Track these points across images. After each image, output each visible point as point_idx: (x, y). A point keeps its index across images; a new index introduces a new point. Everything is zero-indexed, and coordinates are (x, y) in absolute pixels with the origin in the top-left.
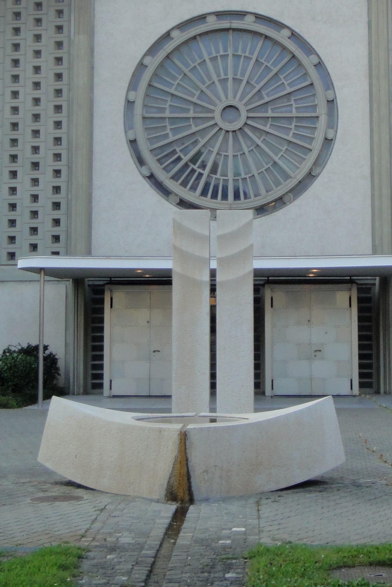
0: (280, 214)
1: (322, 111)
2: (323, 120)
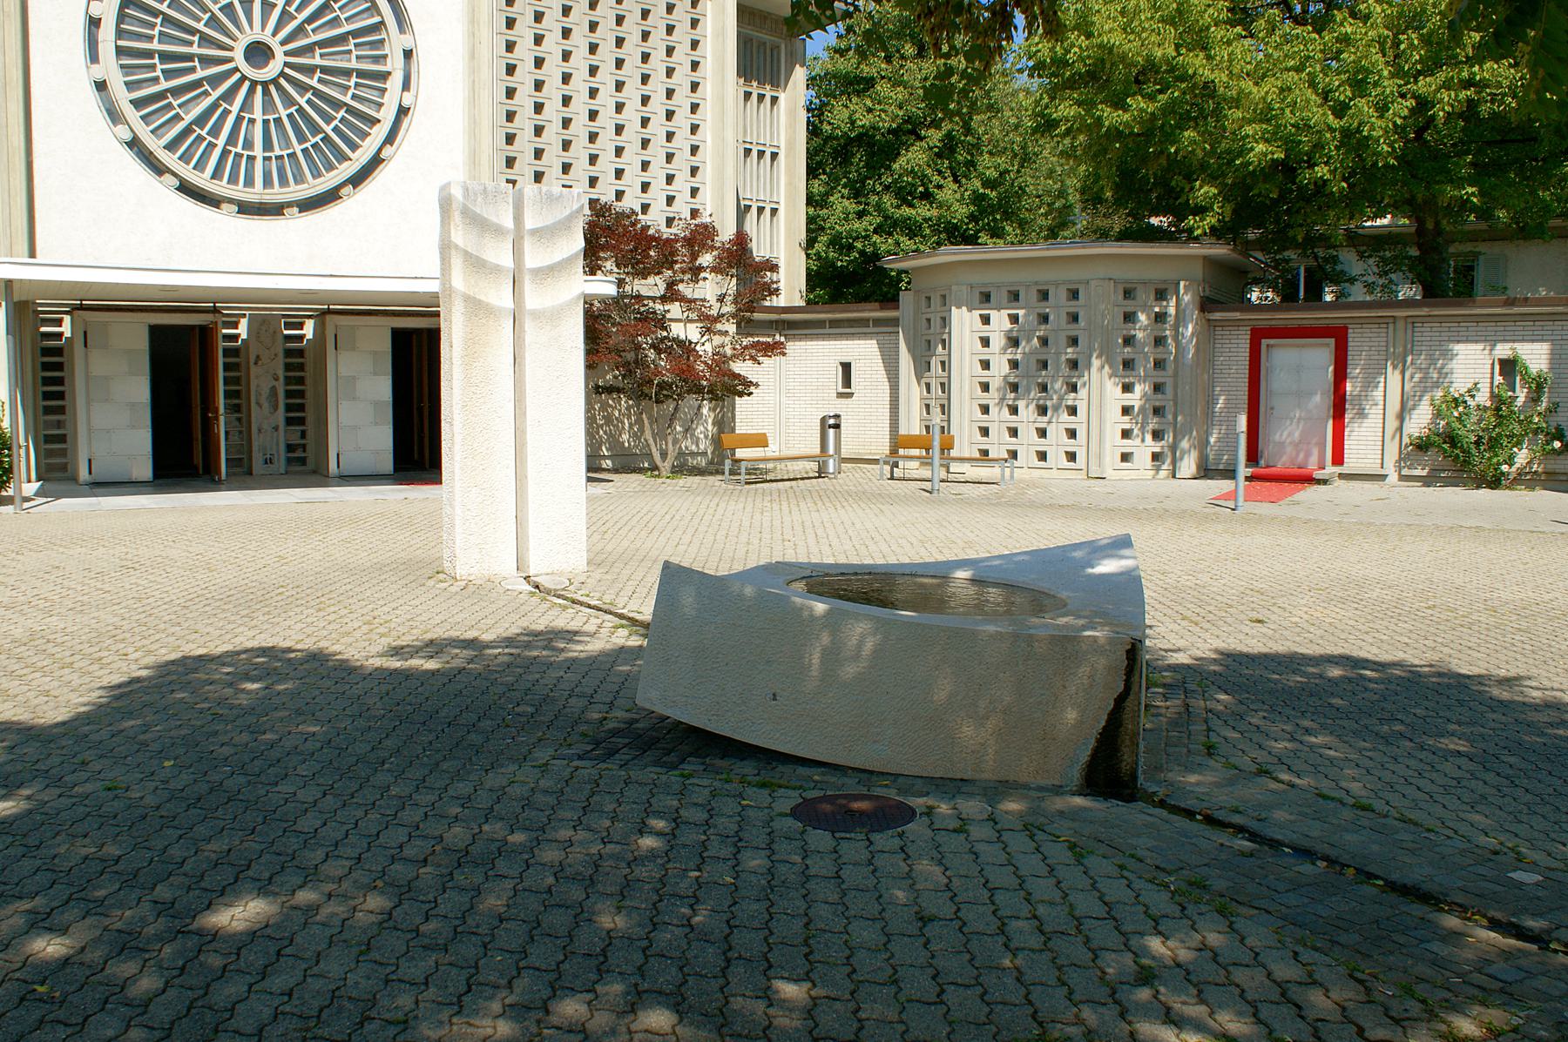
1: (395, 64)
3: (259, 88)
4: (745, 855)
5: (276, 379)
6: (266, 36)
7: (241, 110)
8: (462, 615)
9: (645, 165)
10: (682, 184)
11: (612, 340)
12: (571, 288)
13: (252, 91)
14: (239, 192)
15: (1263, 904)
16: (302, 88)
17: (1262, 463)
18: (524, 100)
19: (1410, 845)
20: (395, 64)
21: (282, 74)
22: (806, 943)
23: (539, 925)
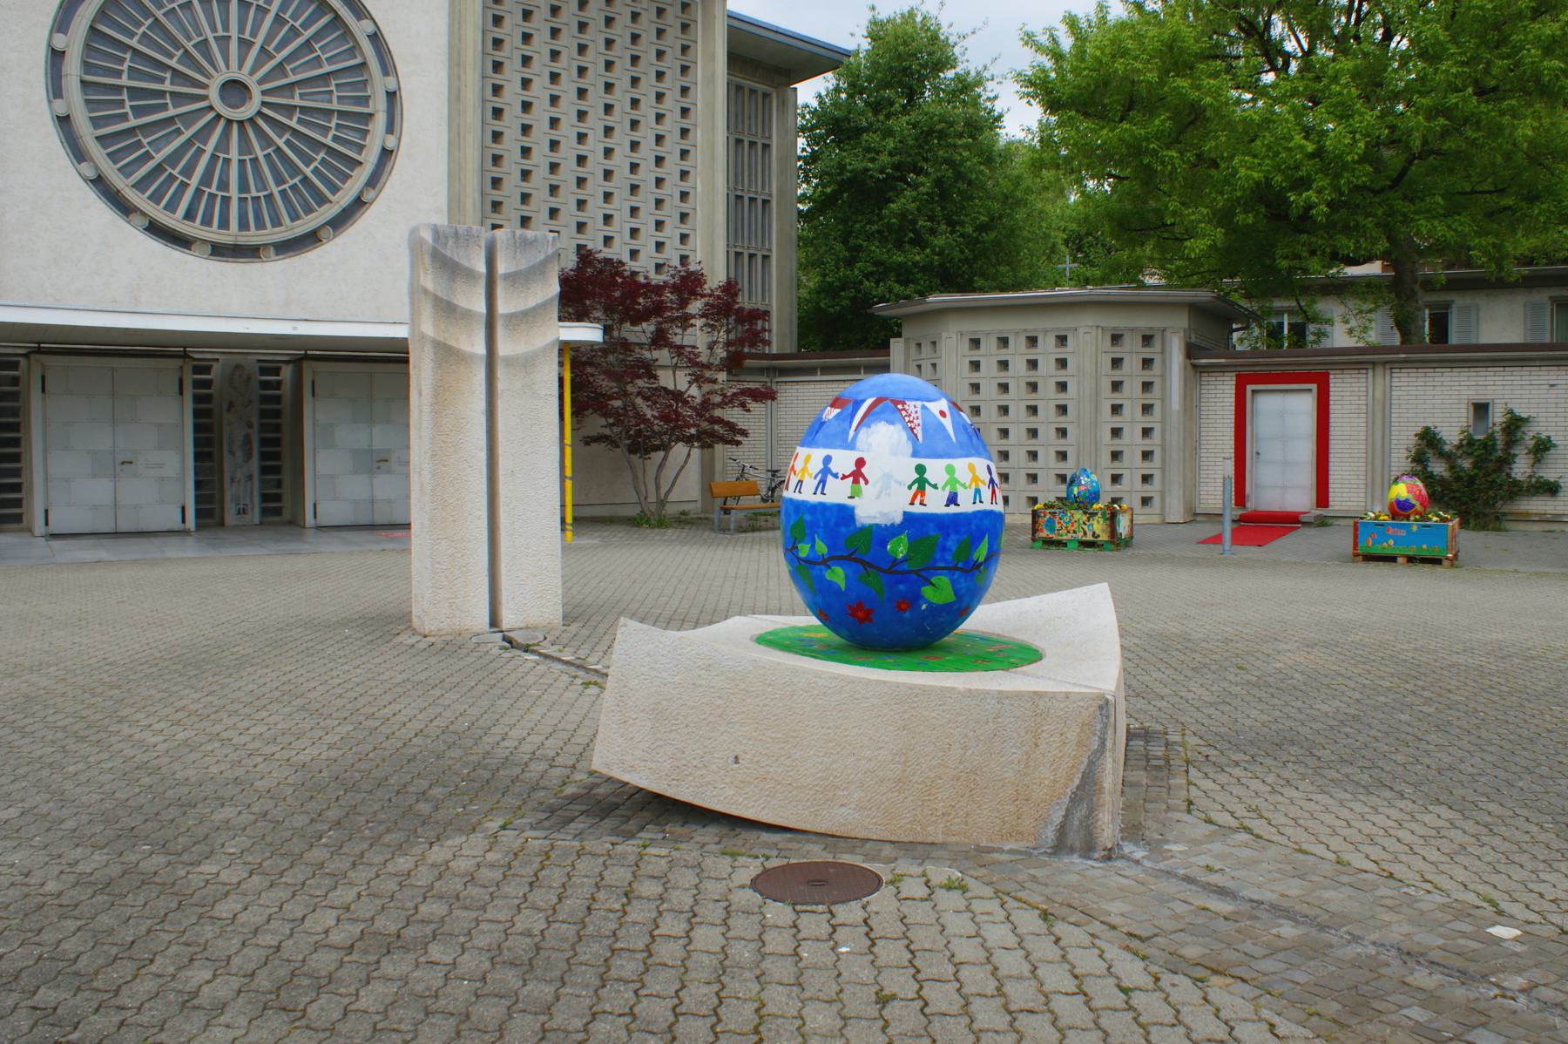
0: (313, 256)
1: (379, 105)
2: (380, 120)
3: (235, 126)
4: (699, 933)
5: (250, 426)
6: (243, 76)
7: (216, 149)
8: (427, 673)
9: (634, 211)
10: (671, 232)
11: (589, 387)
12: (546, 337)
13: (226, 134)
14: (214, 234)
15: (1237, 971)
16: (281, 128)
17: (1248, 505)
18: (511, 144)
19: (1388, 902)
20: (379, 105)
21: (259, 113)
22: (756, 1031)
23: (468, 1016)
